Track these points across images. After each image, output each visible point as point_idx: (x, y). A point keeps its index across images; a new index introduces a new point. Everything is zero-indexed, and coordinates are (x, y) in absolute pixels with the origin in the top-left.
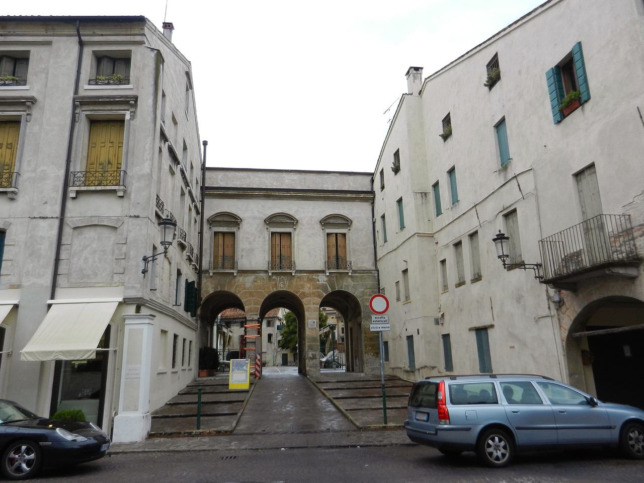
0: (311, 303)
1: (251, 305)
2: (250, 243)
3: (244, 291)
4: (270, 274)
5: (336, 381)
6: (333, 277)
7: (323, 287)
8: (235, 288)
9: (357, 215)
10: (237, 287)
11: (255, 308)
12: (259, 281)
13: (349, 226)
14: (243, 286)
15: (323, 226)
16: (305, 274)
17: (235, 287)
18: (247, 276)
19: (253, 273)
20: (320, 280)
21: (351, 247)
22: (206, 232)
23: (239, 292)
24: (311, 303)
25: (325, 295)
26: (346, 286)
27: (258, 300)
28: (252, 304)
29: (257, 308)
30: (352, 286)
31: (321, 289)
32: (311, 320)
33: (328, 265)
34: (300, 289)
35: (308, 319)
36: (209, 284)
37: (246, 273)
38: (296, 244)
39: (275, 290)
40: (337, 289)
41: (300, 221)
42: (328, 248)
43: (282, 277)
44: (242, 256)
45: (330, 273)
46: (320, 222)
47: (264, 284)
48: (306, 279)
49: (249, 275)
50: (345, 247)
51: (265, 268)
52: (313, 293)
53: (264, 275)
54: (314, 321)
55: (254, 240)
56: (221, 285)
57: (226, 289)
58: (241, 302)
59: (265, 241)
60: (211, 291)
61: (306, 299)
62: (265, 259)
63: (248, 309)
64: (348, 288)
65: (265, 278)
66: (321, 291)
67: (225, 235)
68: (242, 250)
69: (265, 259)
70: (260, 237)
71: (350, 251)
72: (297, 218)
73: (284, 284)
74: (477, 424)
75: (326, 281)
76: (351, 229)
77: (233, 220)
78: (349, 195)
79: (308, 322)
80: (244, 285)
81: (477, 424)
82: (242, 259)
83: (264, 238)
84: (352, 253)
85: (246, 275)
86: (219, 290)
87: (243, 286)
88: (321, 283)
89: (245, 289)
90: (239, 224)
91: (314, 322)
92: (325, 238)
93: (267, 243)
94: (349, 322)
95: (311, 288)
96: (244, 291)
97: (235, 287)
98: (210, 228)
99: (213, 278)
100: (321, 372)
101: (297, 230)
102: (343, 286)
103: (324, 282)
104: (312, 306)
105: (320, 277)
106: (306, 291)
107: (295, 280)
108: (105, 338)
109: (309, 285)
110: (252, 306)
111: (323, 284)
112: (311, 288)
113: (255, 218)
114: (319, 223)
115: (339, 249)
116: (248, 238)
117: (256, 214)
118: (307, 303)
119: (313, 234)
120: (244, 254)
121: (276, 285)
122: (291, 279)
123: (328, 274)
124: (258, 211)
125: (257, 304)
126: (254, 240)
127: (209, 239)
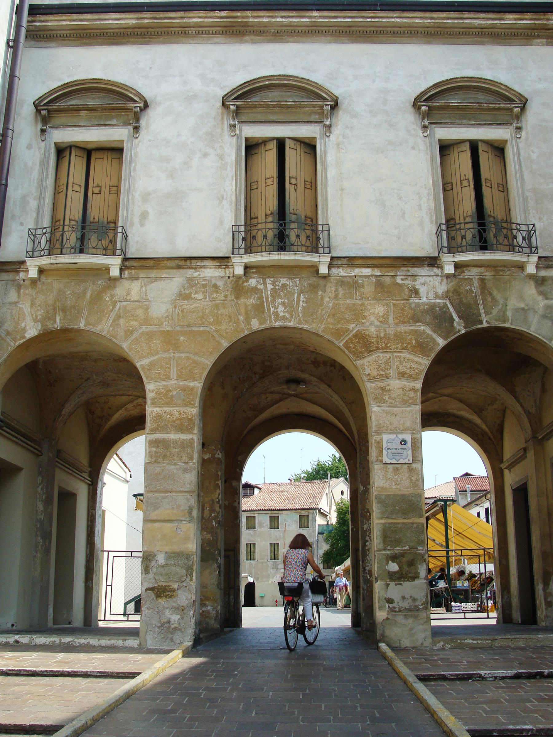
0: (392, 372)
1: (167, 378)
2: (171, 175)
3: (144, 329)
4: (239, 270)
5: (511, 672)
6: (470, 279)
7: (435, 318)
8: (114, 321)
9: (540, 86)
10: (118, 317)
11: (184, 389)
12: (200, 296)
13: (519, 117)
14: (140, 312)
15: (426, 115)
16: (367, 272)
17: (113, 315)
18: (156, 279)
19: (179, 267)
20: (423, 290)
21: (529, 185)
22: (29, 147)
23: (129, 333)
24: (392, 372)
25: (441, 342)
26: (517, 310)
27: (195, 362)
28: (174, 373)
29: (192, 389)
30: (541, 311)
31: (426, 324)
32: (393, 436)
33: (451, 239)
34: (348, 322)
35: (379, 432)
36: (25, 307)
37: (152, 268)
38: (331, 173)
39: (255, 325)
40: (485, 325)
41: (343, 104)
42: (445, 190)
43: (283, 281)
44: (144, 216)
45: (457, 266)
46: (414, 105)
47: (217, 306)
48: (368, 289)
49: (164, 274)
50: (504, 188)
51: (224, 250)
52: (399, 337)
53: (219, 273)
54: (402, 437)
55: (187, 164)
56: (64, 310)
57: (82, 325)
58: (135, 368)
59: (224, 167)
60: (32, 332)
61: (373, 357)
62: (221, 222)
63: (158, 393)
64: (525, 320)
65: (220, 283)
66: (429, 331)
67: (94, 156)
68: (146, 197)
69: (221, 222)
70: (205, 155)
71: (525, 199)
72: (337, 92)
73: (290, 307)
74: (350, 567)
75: (446, 295)
76: (523, 124)
77: (115, 104)
78: (510, 19)
79: (379, 443)
80: (147, 309)
81: (350, 567)
82: (142, 225)
83: (221, 157)
84: (531, 203)
85: (153, 274)
86: (58, 325)
87: (140, 312)
88: (424, 300)
89: (147, 322)
90: (137, 118)
91: (403, 442)
92: (432, 158)
93: (231, 171)
94: (506, 472)
95: (391, 320)
96: (144, 329)
97: (113, 315)
98: (43, 131)
99: (39, 285)
100: (433, 623)
101: (337, 131)
102: (509, 314)
103: (437, 296)
104: (395, 384)
105: (422, 280)
106: (373, 331)
107: (331, 289)
108: (460, 590)
109: (380, 310)
110: (173, 382)
111: (433, 307)
112: (391, 320)
113: (191, 98)
114: (411, 109)
115: (486, 191)
116: (167, 160)
117: (197, 86)
118: (375, 373)
119: (390, 143)
120: (151, 209)
121: (259, 309)
122: (314, 288)
123: (449, 269)
124: (202, 77)
125: (191, 377)
126: (187, 164)
127: (37, 167)
